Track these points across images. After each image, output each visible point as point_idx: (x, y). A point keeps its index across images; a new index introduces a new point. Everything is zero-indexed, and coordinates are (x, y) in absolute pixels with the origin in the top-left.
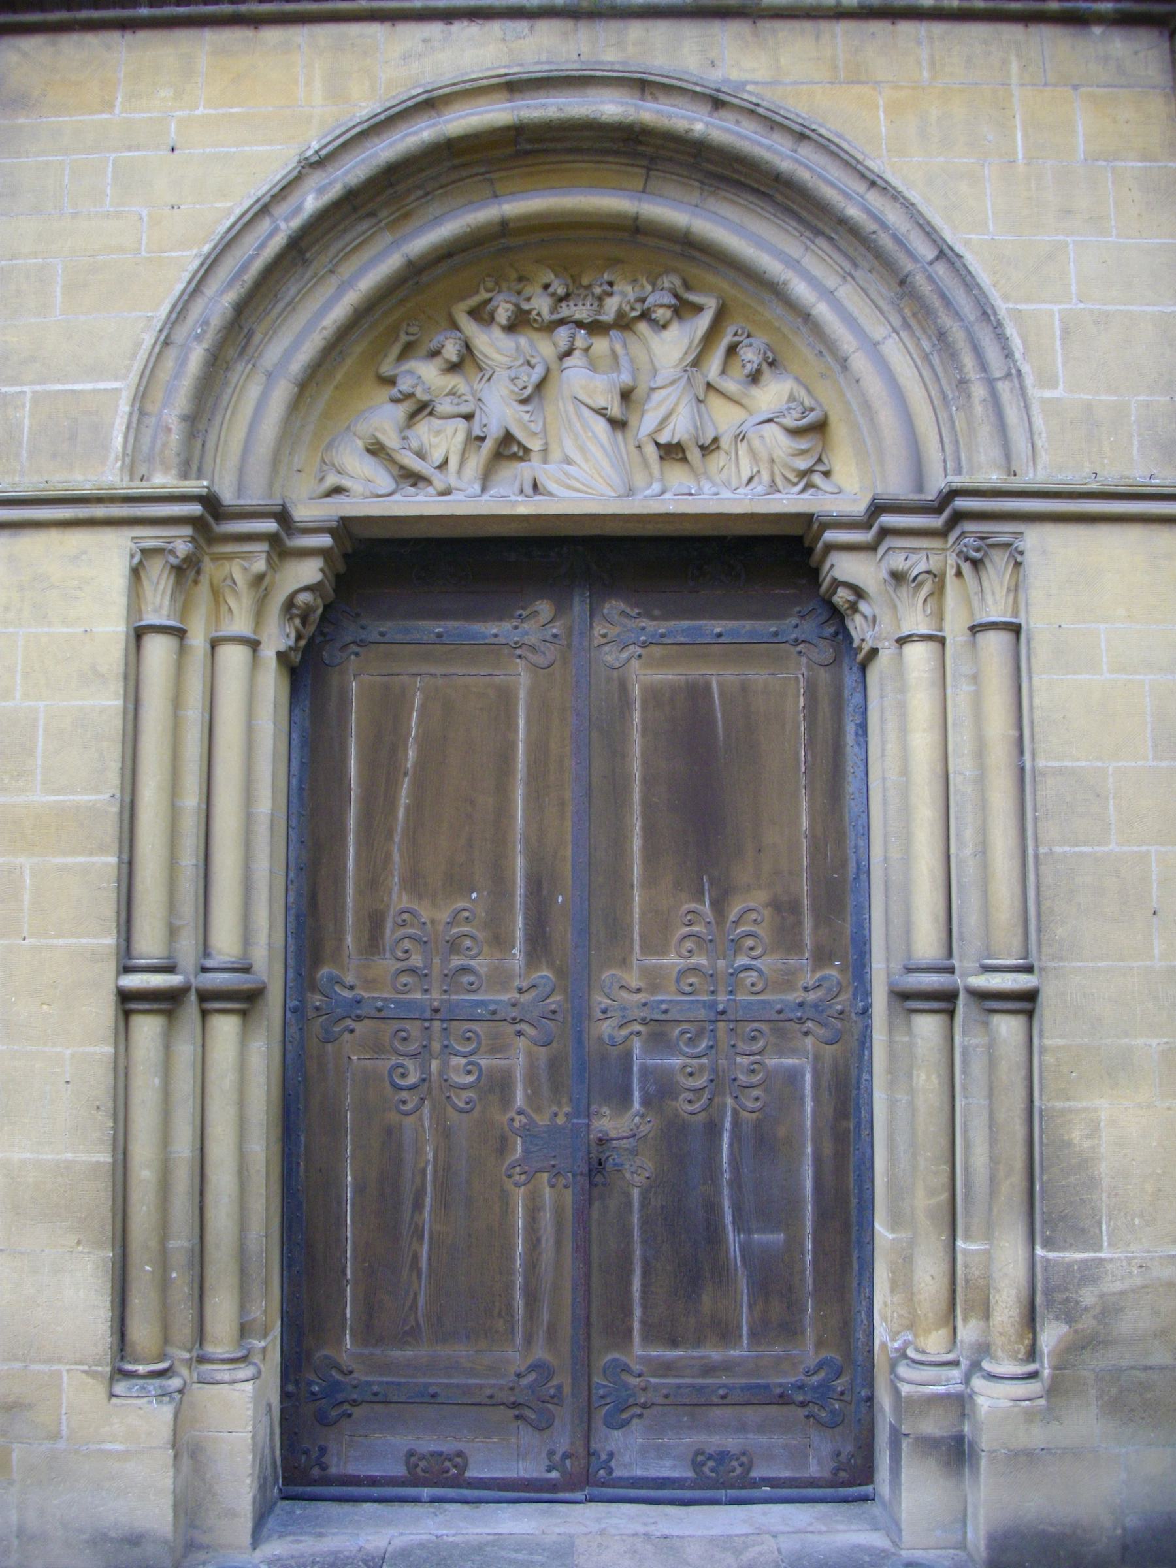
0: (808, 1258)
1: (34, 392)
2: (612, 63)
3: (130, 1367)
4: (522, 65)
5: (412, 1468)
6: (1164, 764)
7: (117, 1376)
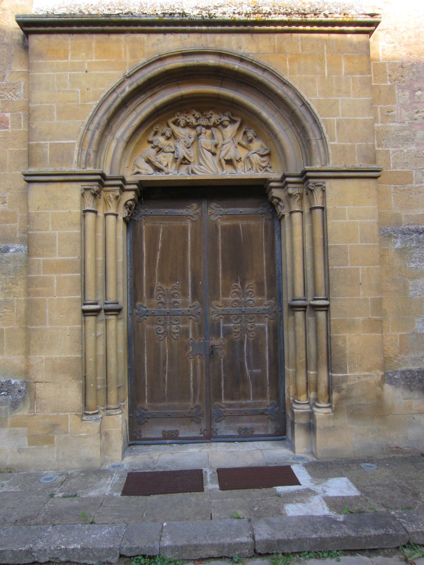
0: (268, 376)
1: (50, 143)
2: (212, 48)
3: (87, 412)
4: (186, 48)
5: (164, 435)
6: (363, 244)
7: (84, 415)
